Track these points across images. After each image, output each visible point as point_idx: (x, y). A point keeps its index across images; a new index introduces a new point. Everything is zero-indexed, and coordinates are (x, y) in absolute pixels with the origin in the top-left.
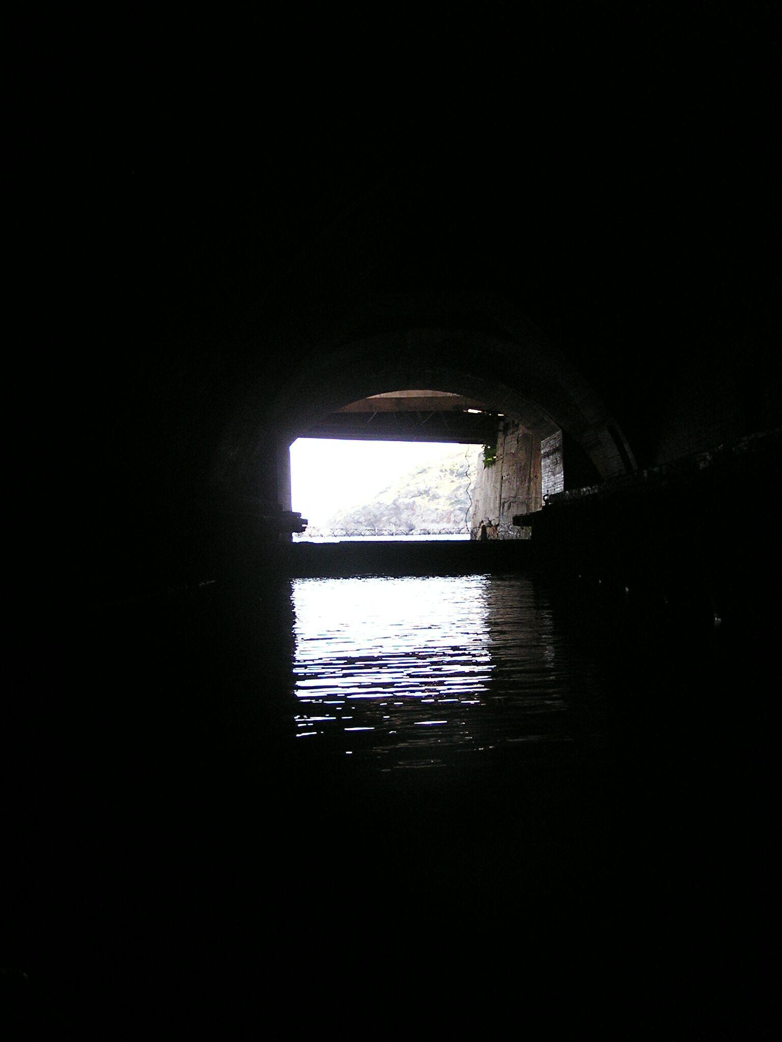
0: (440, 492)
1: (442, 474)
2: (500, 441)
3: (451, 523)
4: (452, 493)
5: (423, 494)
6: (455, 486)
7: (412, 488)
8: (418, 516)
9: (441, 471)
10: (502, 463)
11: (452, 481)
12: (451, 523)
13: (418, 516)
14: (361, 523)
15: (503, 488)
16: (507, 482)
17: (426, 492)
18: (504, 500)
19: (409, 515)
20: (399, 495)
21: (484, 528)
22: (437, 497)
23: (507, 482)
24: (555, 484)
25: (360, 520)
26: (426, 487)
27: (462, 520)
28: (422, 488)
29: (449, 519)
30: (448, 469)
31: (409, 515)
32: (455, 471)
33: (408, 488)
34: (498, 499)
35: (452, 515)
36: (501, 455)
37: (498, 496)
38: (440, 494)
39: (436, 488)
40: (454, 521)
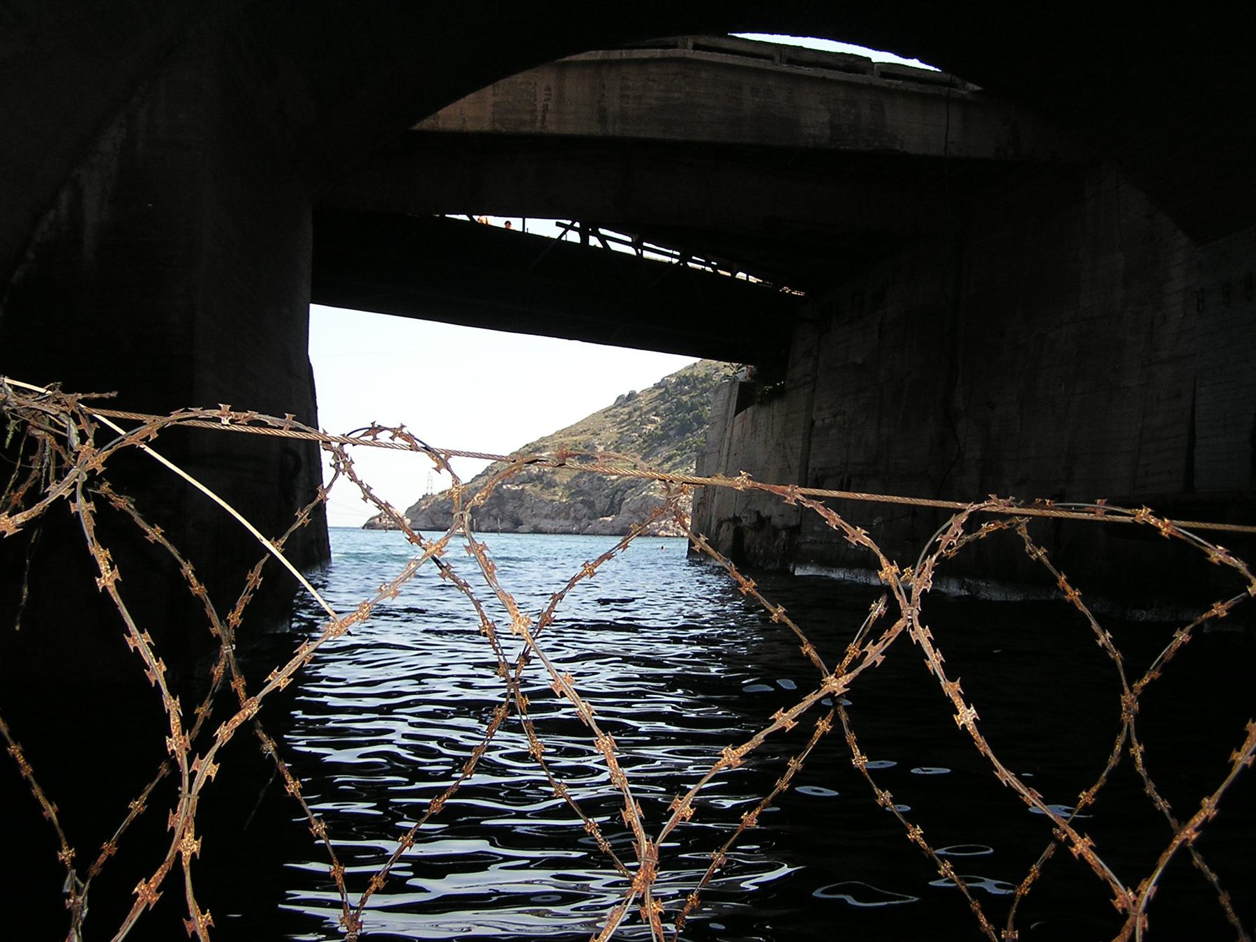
3: (570, 520)
4: (572, 480)
8: (527, 508)
12: (570, 520)
13: (527, 508)
21: (739, 534)
22: (553, 484)
26: (539, 471)
27: (585, 516)
29: (568, 514)
31: (515, 507)
35: (572, 509)
38: (558, 481)
40: (575, 517)
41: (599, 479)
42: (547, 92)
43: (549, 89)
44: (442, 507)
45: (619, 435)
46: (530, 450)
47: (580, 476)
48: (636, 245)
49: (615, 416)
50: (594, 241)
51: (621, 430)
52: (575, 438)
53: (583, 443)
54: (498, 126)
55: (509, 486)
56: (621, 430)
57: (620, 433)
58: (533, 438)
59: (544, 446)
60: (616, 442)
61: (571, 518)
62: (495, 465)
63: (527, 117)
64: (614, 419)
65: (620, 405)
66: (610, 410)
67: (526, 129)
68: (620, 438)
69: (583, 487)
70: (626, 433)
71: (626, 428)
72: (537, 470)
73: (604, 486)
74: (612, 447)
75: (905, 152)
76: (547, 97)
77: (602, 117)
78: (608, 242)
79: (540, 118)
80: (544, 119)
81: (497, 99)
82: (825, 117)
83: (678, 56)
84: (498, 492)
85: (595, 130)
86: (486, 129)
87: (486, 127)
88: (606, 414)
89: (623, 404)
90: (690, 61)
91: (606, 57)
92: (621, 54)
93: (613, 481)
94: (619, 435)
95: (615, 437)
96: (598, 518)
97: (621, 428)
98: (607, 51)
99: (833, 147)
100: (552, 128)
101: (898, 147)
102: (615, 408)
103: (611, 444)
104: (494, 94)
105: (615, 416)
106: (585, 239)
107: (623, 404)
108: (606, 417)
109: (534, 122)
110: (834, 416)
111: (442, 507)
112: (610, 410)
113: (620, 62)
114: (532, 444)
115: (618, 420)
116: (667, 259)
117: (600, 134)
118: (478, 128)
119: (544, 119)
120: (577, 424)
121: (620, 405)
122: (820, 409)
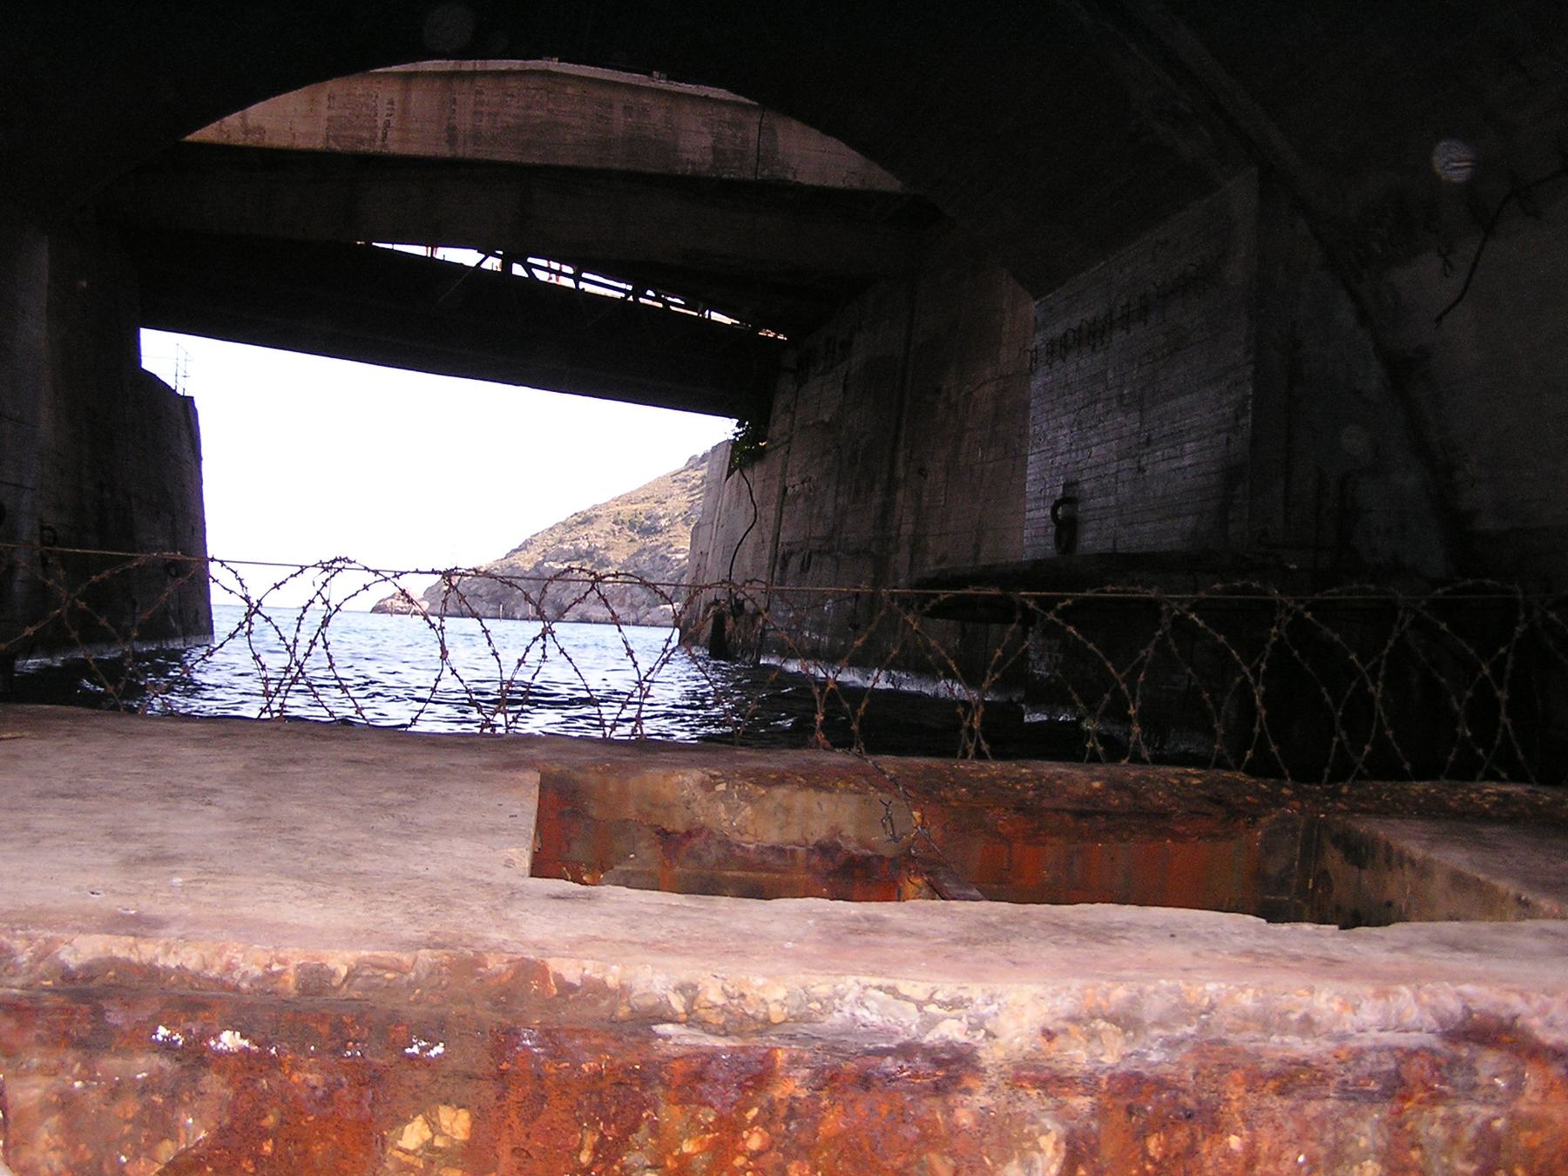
0: (611, 555)
1: (616, 528)
2: (780, 401)
3: (626, 608)
4: (629, 559)
5: (583, 557)
6: (635, 548)
7: (566, 547)
8: (573, 591)
9: (615, 523)
10: (788, 452)
11: (631, 541)
12: (626, 608)
13: (573, 591)
14: (481, 596)
15: (785, 517)
16: (800, 501)
17: (589, 554)
18: (787, 549)
19: (558, 590)
20: (545, 556)
21: (719, 621)
22: (606, 563)
23: (800, 501)
24: (1148, 442)
25: (480, 592)
26: (590, 546)
27: (644, 603)
28: (583, 545)
29: (623, 600)
30: (627, 519)
31: (558, 590)
32: (638, 525)
33: (560, 546)
34: (768, 545)
35: (628, 594)
36: (785, 434)
37: (769, 537)
38: (612, 559)
39: (607, 548)
40: (631, 604)
41: (663, 557)
42: (389, 106)
43: (391, 103)
44: (469, 588)
45: (689, 505)
46: (580, 520)
47: (640, 552)
48: (577, 278)
49: (685, 481)
50: (518, 270)
51: (692, 498)
52: (635, 507)
53: (644, 513)
54: (333, 145)
55: (552, 564)
56: (692, 498)
57: (690, 502)
58: (583, 505)
59: (596, 516)
60: (686, 513)
61: (627, 605)
62: (536, 538)
63: (365, 134)
64: (684, 484)
65: (692, 467)
66: (679, 473)
67: (362, 148)
68: (690, 508)
69: (642, 566)
70: (697, 502)
71: (698, 496)
72: (587, 544)
73: (669, 567)
74: (680, 518)
75: (798, 182)
76: (389, 112)
77: (452, 135)
78: (534, 270)
79: (380, 134)
80: (385, 135)
81: (333, 112)
82: (707, 141)
83: (540, 68)
84: (538, 571)
85: (445, 151)
86: (319, 147)
87: (319, 144)
88: (675, 478)
89: (696, 467)
90: (556, 74)
91: (457, 68)
92: (475, 64)
93: (679, 560)
94: (689, 505)
95: (684, 507)
96: (658, 605)
97: (692, 495)
98: (458, 61)
99: (714, 175)
100: (394, 148)
101: (790, 177)
102: (686, 470)
103: (680, 515)
104: (329, 107)
105: (685, 481)
106: (507, 266)
107: (696, 467)
108: (675, 481)
109: (373, 140)
110: (803, 483)
111: (469, 588)
112: (679, 473)
113: (474, 74)
114: (582, 513)
115: (689, 485)
116: (610, 293)
117: (448, 156)
118: (311, 146)
119: (385, 135)
120: (640, 489)
121: (692, 467)
122: (792, 475)
